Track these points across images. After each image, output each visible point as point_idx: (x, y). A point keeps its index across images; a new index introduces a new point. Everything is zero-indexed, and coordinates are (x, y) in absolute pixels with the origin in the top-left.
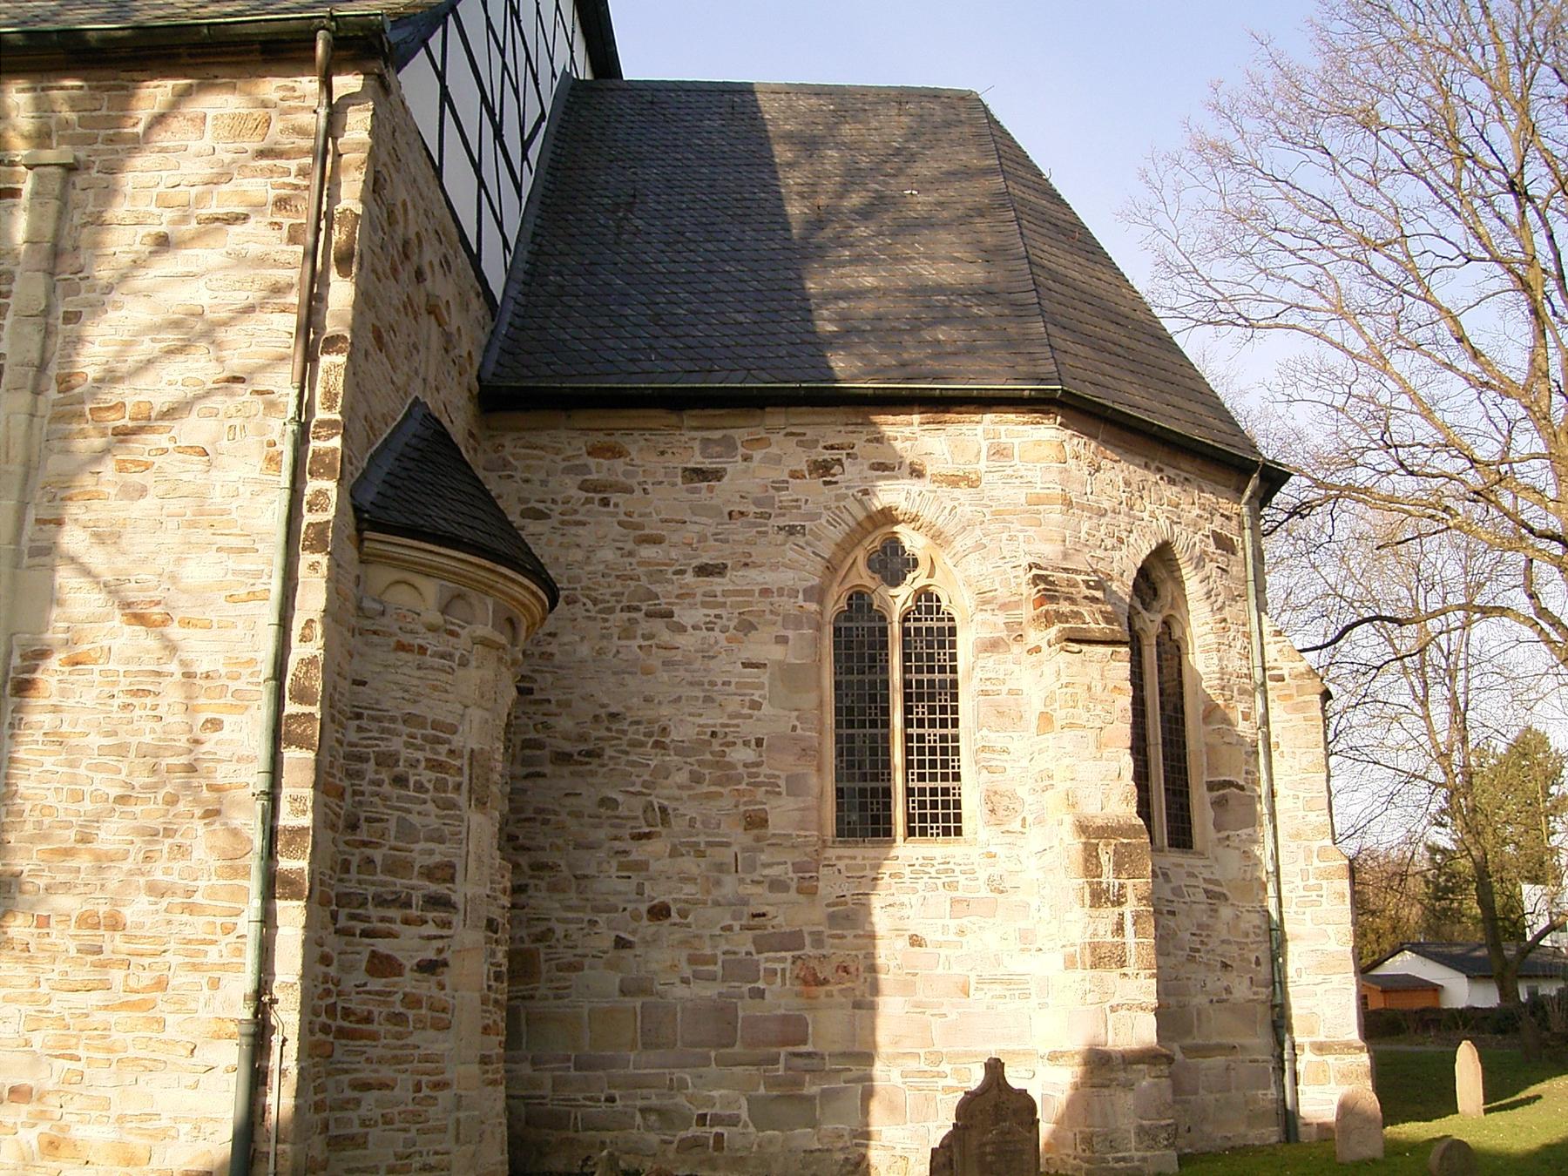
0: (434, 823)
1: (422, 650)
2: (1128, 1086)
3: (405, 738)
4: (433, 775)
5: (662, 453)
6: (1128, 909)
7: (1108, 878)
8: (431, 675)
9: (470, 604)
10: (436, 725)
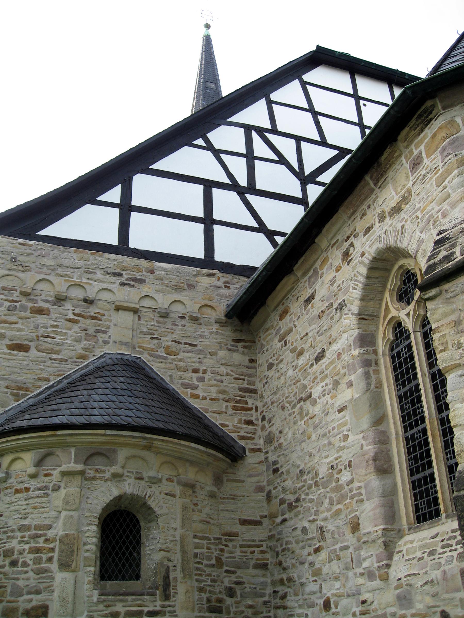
0: (32, 583)
1: (27, 490)
3: (19, 539)
4: (32, 556)
5: (297, 299)
8: (32, 501)
9: (57, 456)
10: (37, 527)
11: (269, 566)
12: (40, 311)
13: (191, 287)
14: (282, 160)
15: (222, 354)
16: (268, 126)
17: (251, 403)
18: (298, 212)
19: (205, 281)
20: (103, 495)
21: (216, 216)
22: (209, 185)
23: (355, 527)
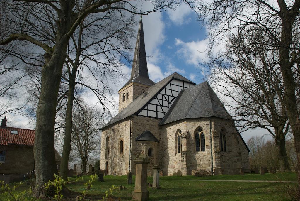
2: (183, 170)
6: (184, 157)
7: (183, 155)
11: (266, 174)
12: (139, 125)
13: (155, 121)
14: (166, 100)
15: (158, 130)
16: (165, 94)
17: (161, 136)
18: (168, 109)
19: (157, 120)
20: (149, 147)
21: (158, 111)
22: (157, 105)
23: (173, 152)
